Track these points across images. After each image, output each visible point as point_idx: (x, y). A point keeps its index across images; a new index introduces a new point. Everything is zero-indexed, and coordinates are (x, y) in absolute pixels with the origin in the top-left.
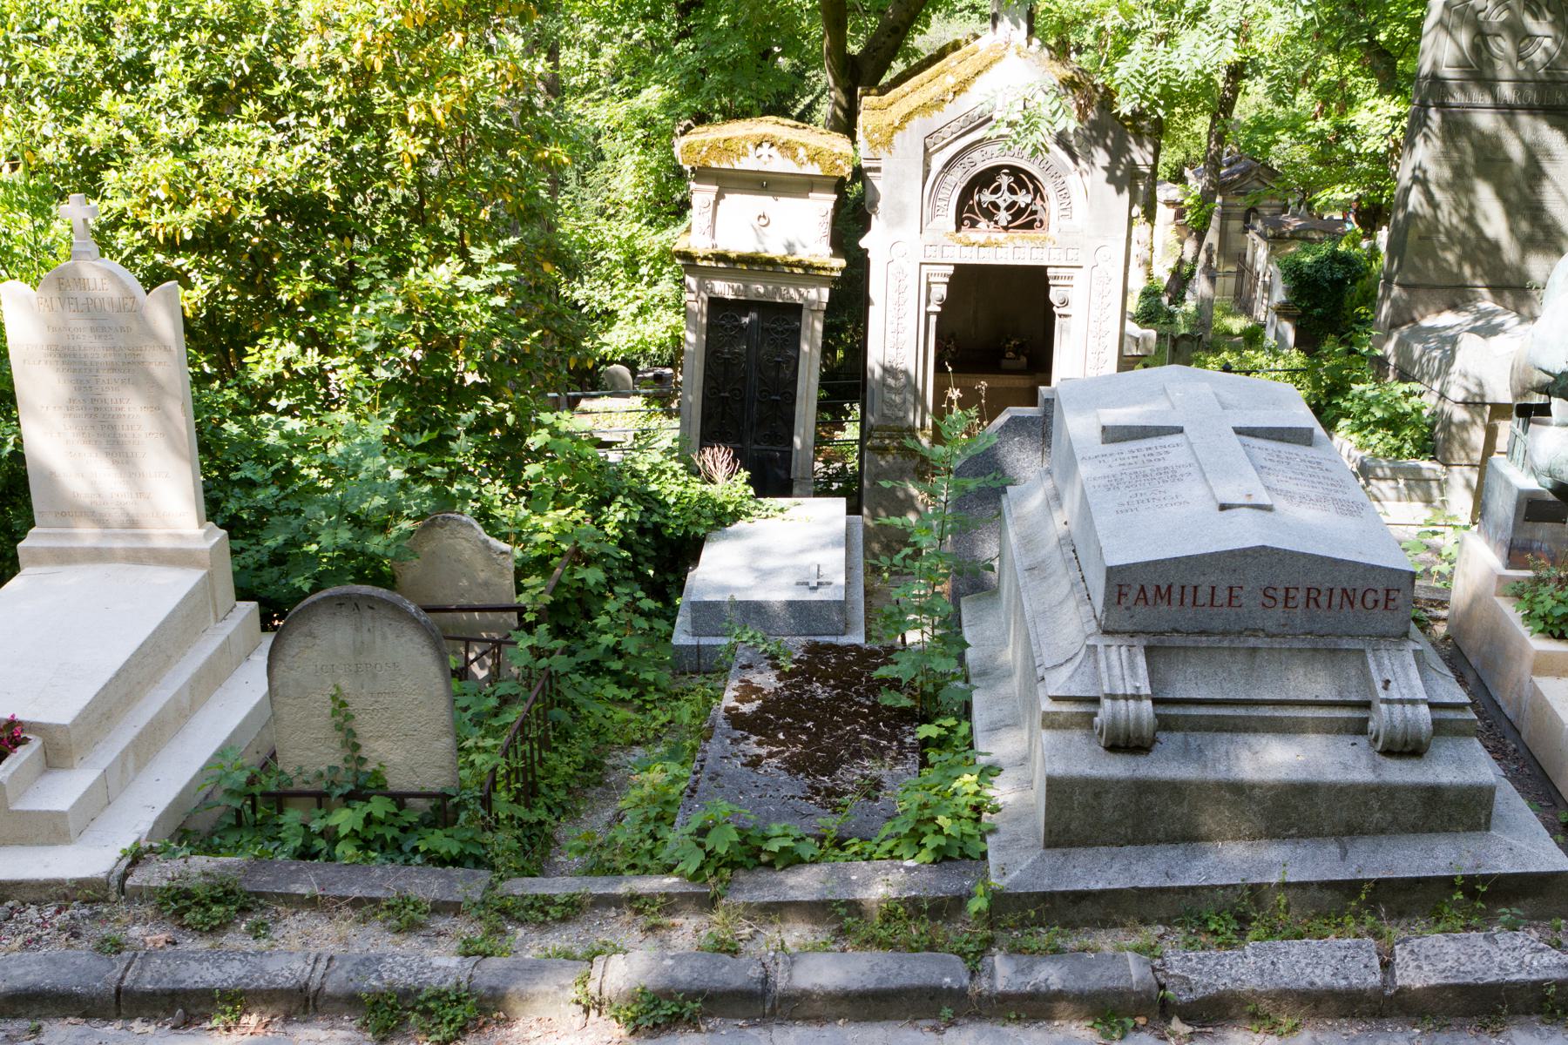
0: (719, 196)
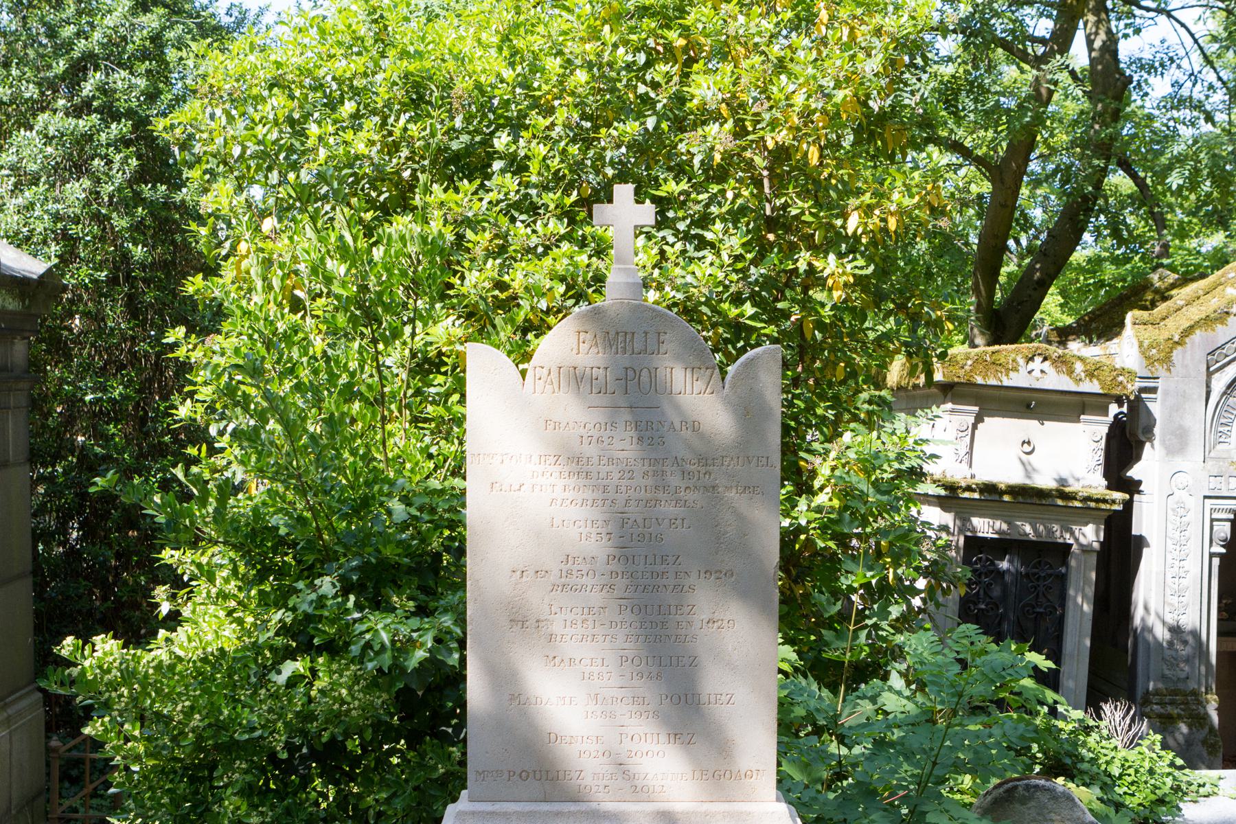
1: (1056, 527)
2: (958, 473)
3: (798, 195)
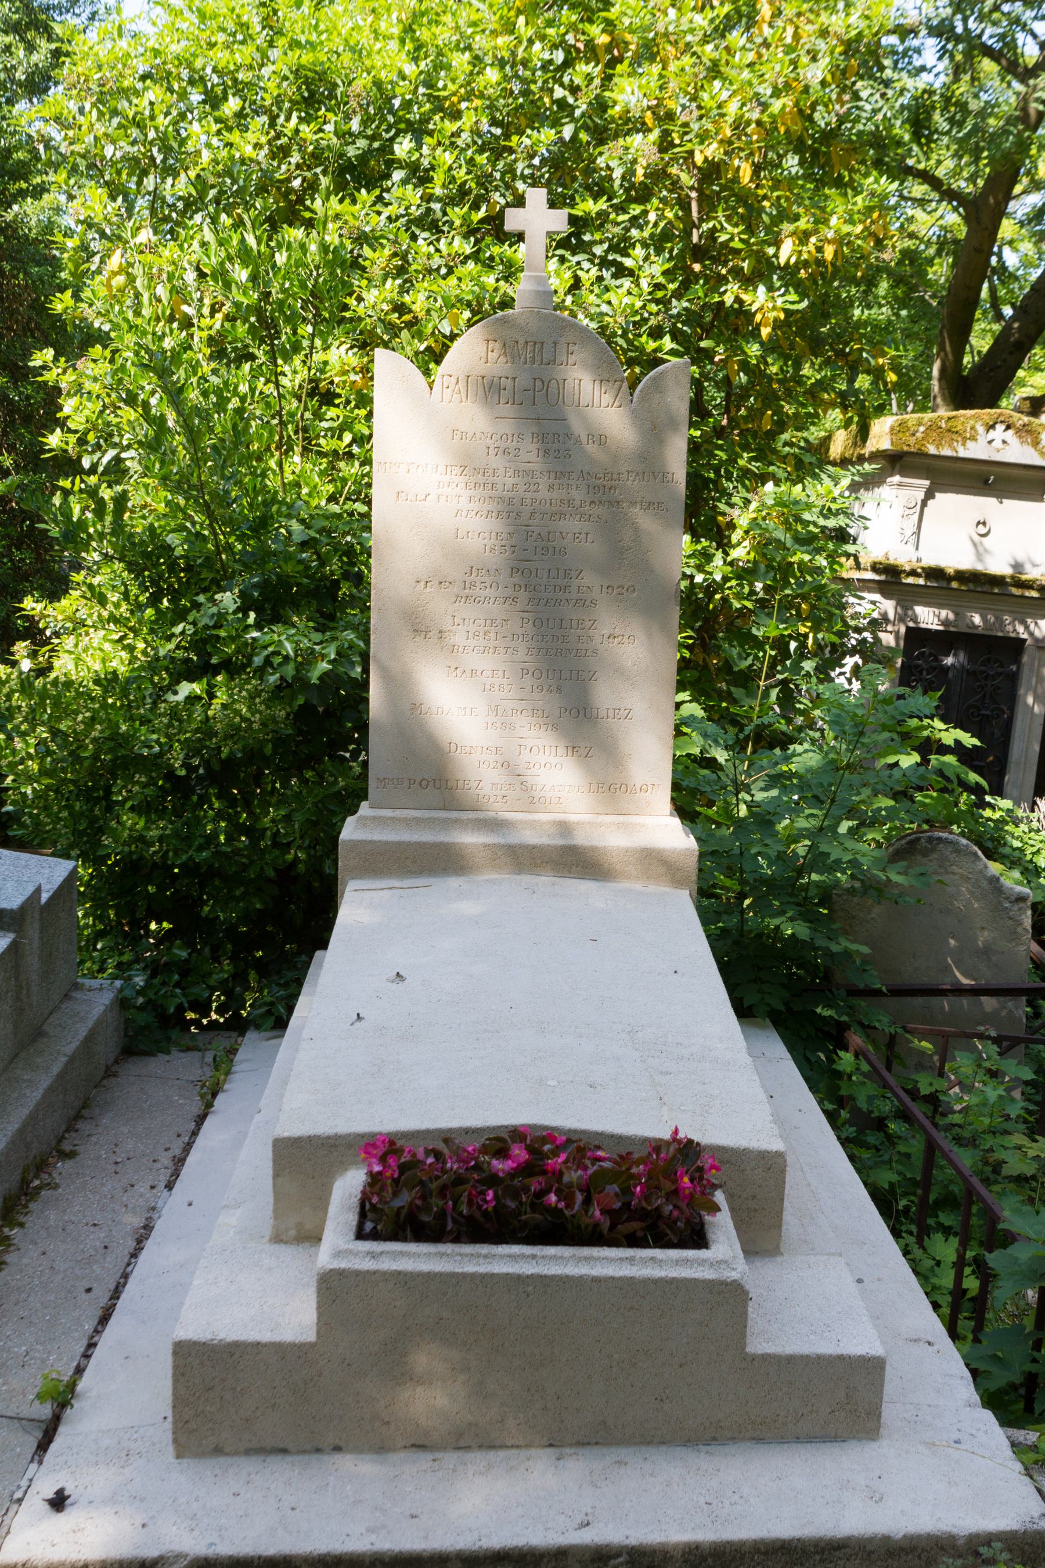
0: (929, 495)
1: (1008, 619)
2: (903, 556)
3: (729, 219)
